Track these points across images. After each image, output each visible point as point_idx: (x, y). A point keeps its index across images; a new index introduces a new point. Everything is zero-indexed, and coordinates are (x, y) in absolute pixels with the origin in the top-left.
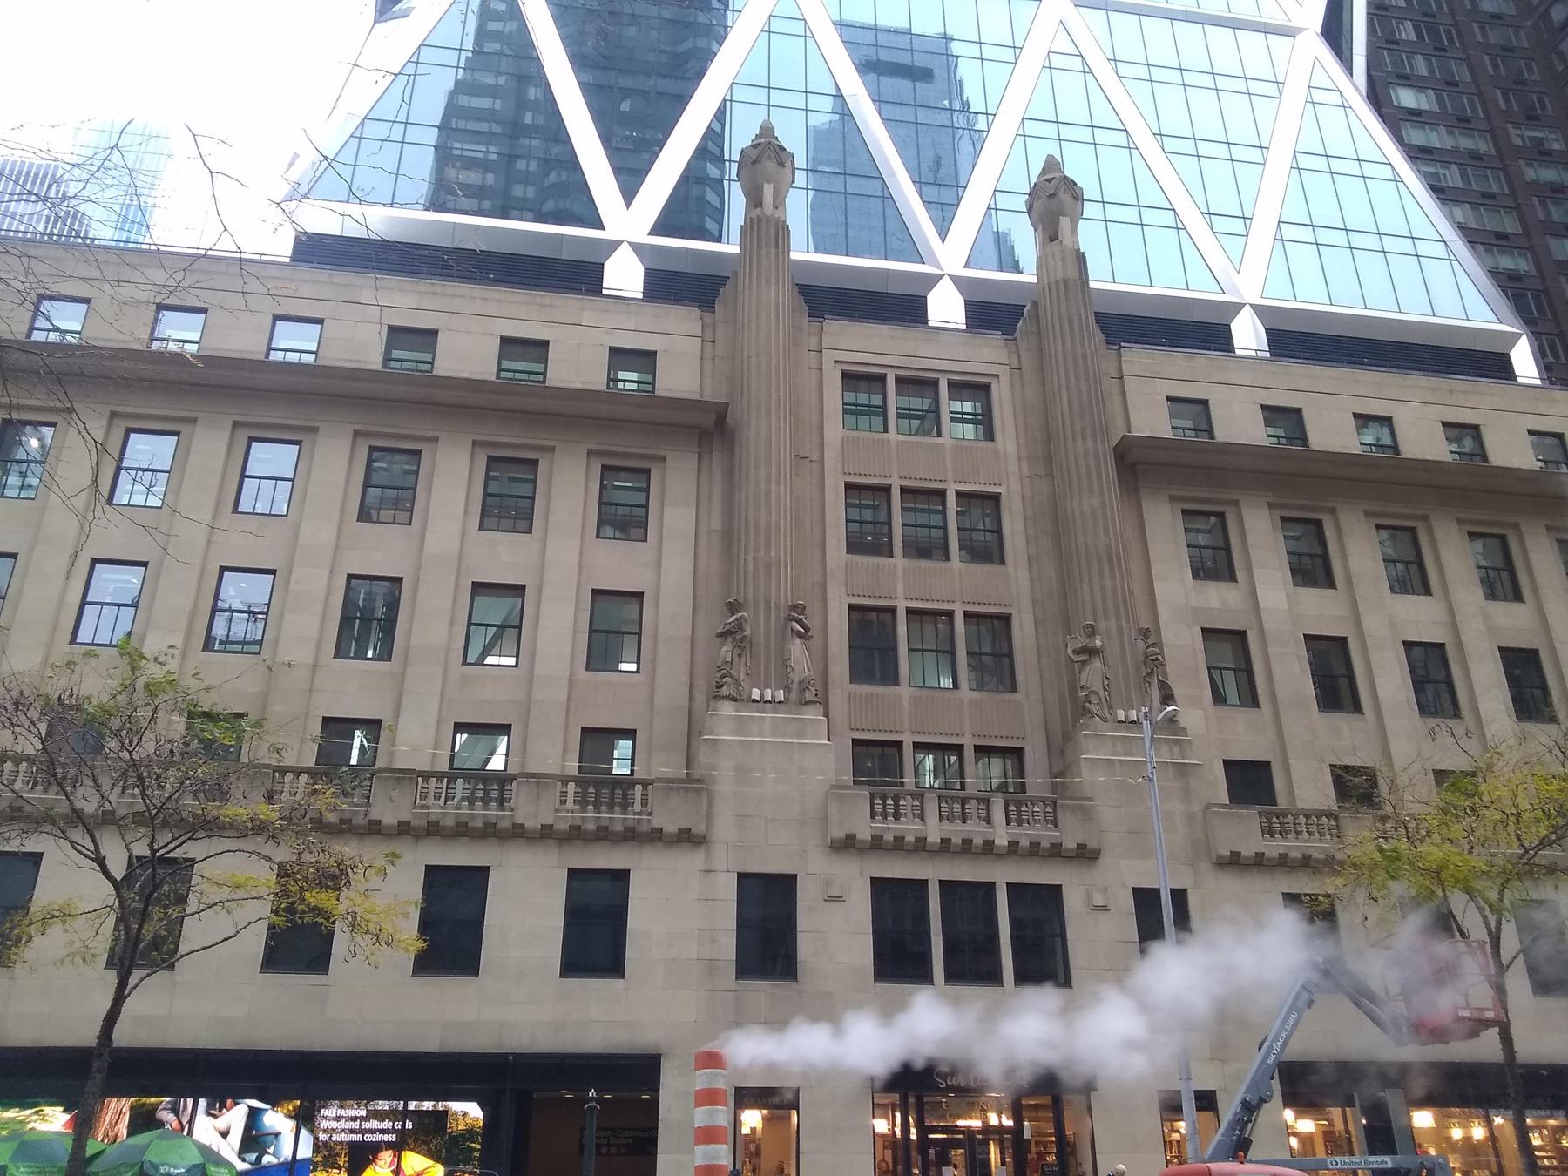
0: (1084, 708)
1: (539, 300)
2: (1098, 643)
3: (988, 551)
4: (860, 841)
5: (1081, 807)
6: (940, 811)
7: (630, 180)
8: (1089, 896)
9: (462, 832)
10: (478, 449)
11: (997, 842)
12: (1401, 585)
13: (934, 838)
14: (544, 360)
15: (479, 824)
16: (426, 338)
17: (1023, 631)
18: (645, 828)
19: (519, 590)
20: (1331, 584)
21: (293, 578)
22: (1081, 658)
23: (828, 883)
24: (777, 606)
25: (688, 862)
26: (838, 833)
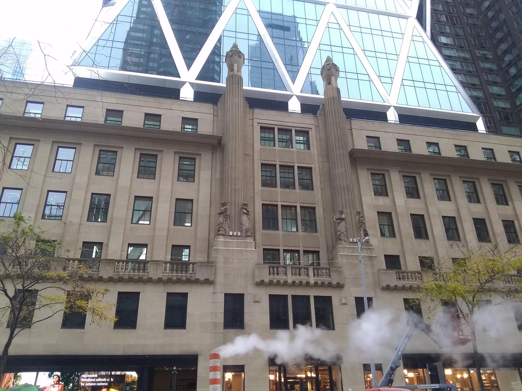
3: (308, 186)
7: (189, 61)
8: (341, 300)
10: (137, 151)
13: (290, 281)
14: (160, 121)
16: (119, 113)
17: (319, 212)
18: (193, 279)
21: (73, 194)
24: (238, 205)
25: (208, 290)
26: (258, 280)
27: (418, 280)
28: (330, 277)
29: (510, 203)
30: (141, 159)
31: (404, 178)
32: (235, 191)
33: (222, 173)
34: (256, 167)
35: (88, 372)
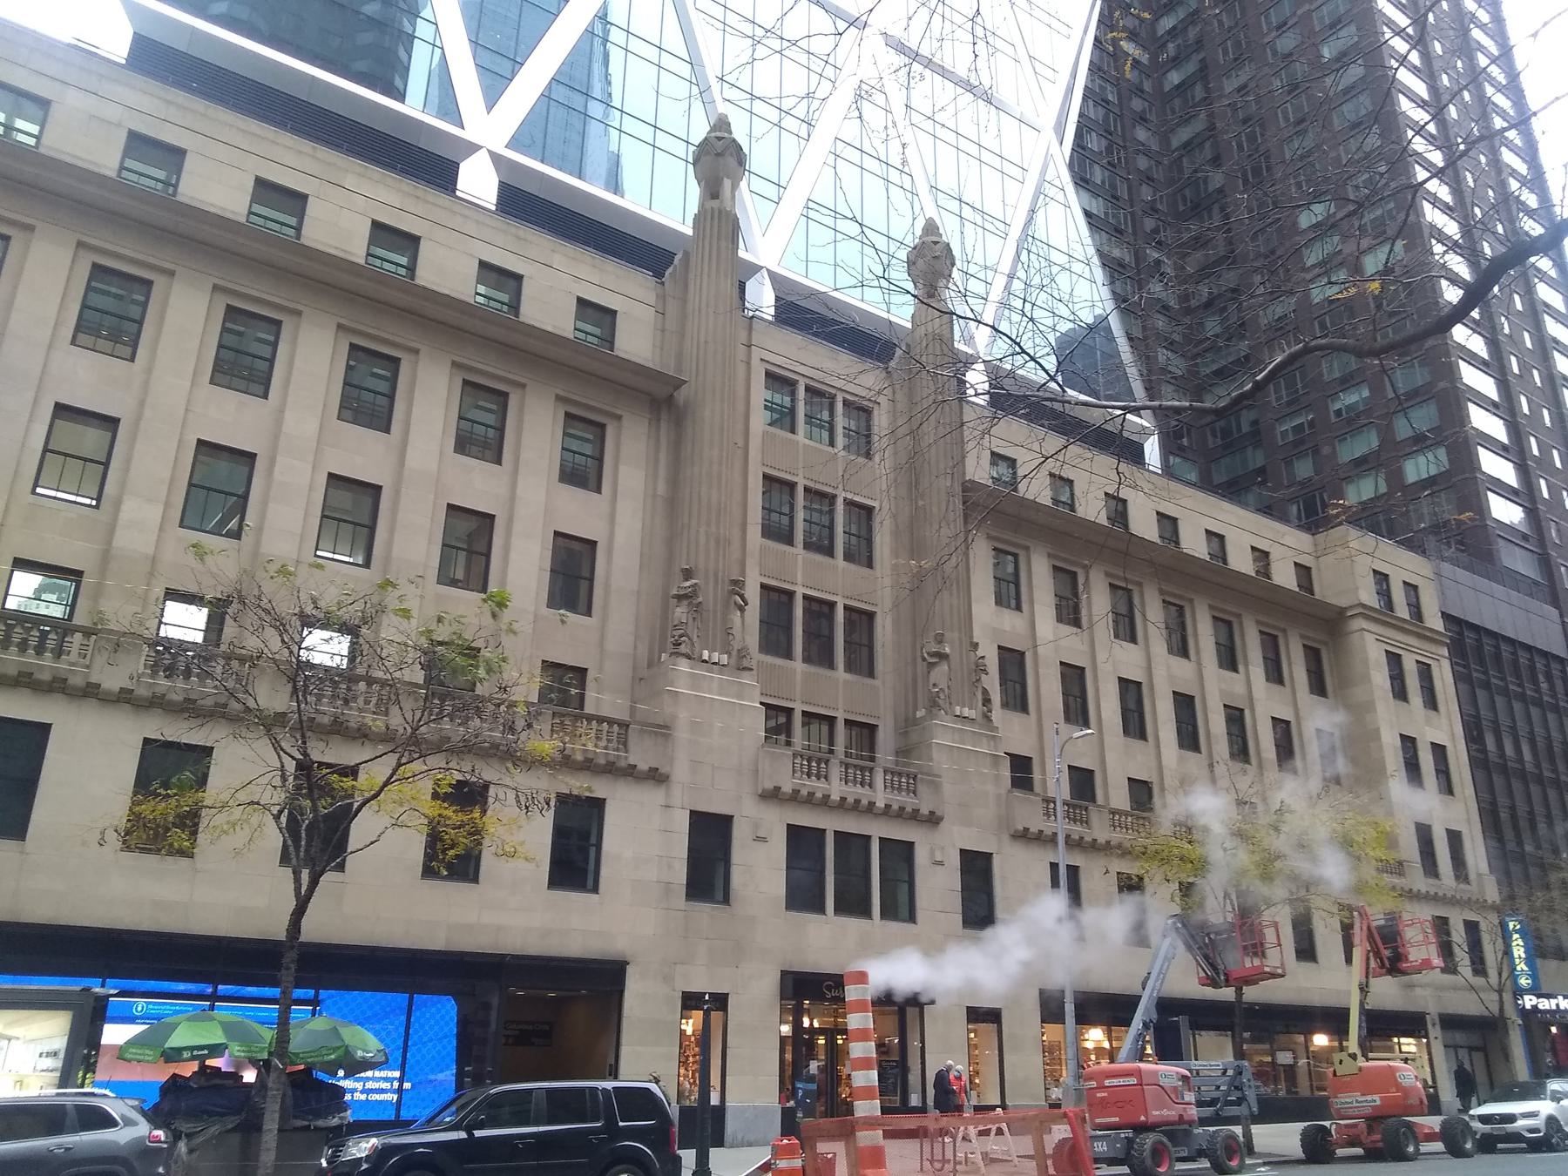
0: (934, 702)
1: (513, 230)
2: (947, 650)
3: (862, 554)
5: (933, 782)
7: (495, 83)
10: (82, 253)
11: (877, 804)
13: (787, 788)
14: (301, 215)
15: (46, 676)
16: (296, 201)
17: (884, 631)
18: (623, 764)
19: (111, 423)
20: (1019, 608)
21: (277, 469)
23: (756, 826)
24: (723, 581)
25: (651, 796)
26: (769, 785)
27: (1130, 831)
29: (1241, 668)
30: (93, 284)
32: (718, 542)
33: (674, 482)
34: (751, 479)
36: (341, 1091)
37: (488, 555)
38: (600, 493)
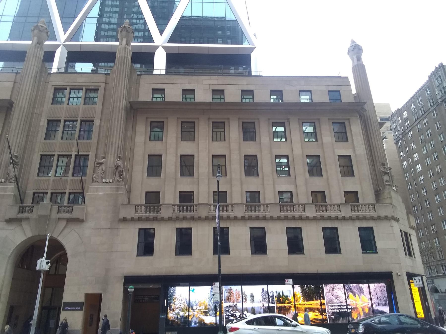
4: (389, 217)
6: (316, 209)
9: (147, 219)
12: (338, 140)
22: (98, 165)
28: (375, 211)
31: (334, 124)
35: (344, 283)
36: (435, 318)
37: (320, 166)
38: (317, 141)
